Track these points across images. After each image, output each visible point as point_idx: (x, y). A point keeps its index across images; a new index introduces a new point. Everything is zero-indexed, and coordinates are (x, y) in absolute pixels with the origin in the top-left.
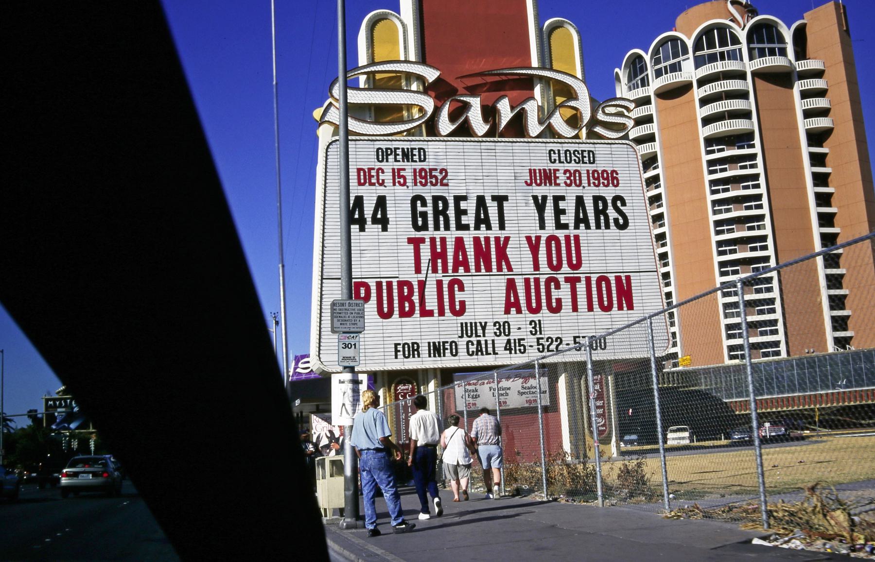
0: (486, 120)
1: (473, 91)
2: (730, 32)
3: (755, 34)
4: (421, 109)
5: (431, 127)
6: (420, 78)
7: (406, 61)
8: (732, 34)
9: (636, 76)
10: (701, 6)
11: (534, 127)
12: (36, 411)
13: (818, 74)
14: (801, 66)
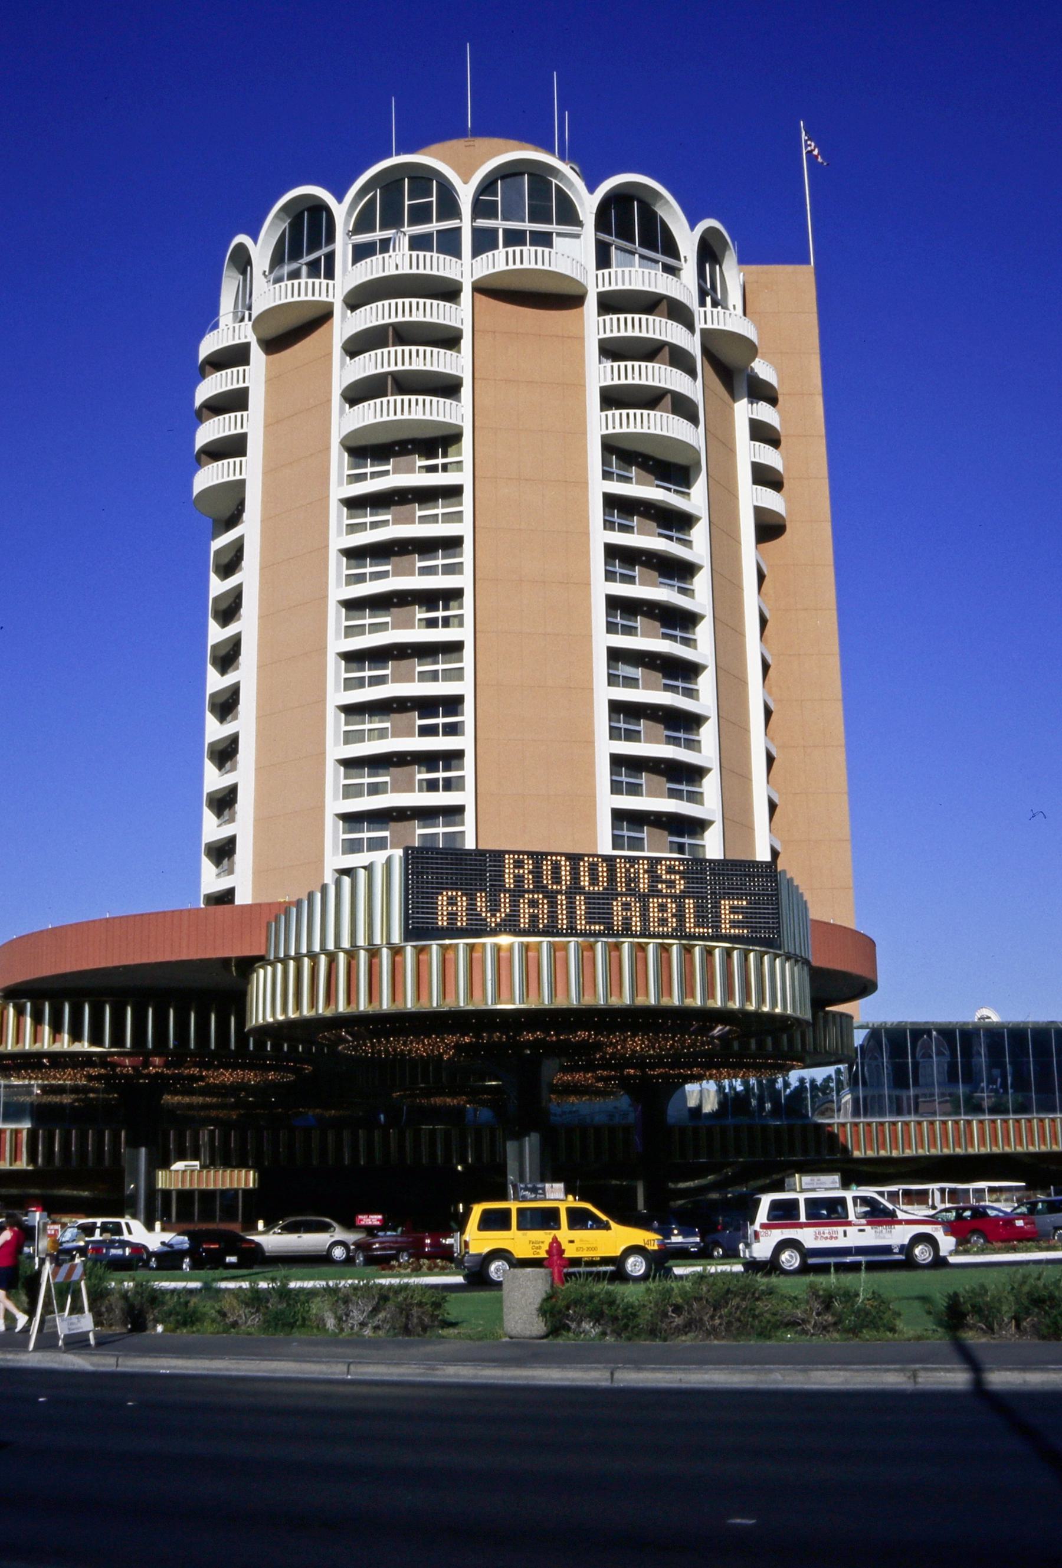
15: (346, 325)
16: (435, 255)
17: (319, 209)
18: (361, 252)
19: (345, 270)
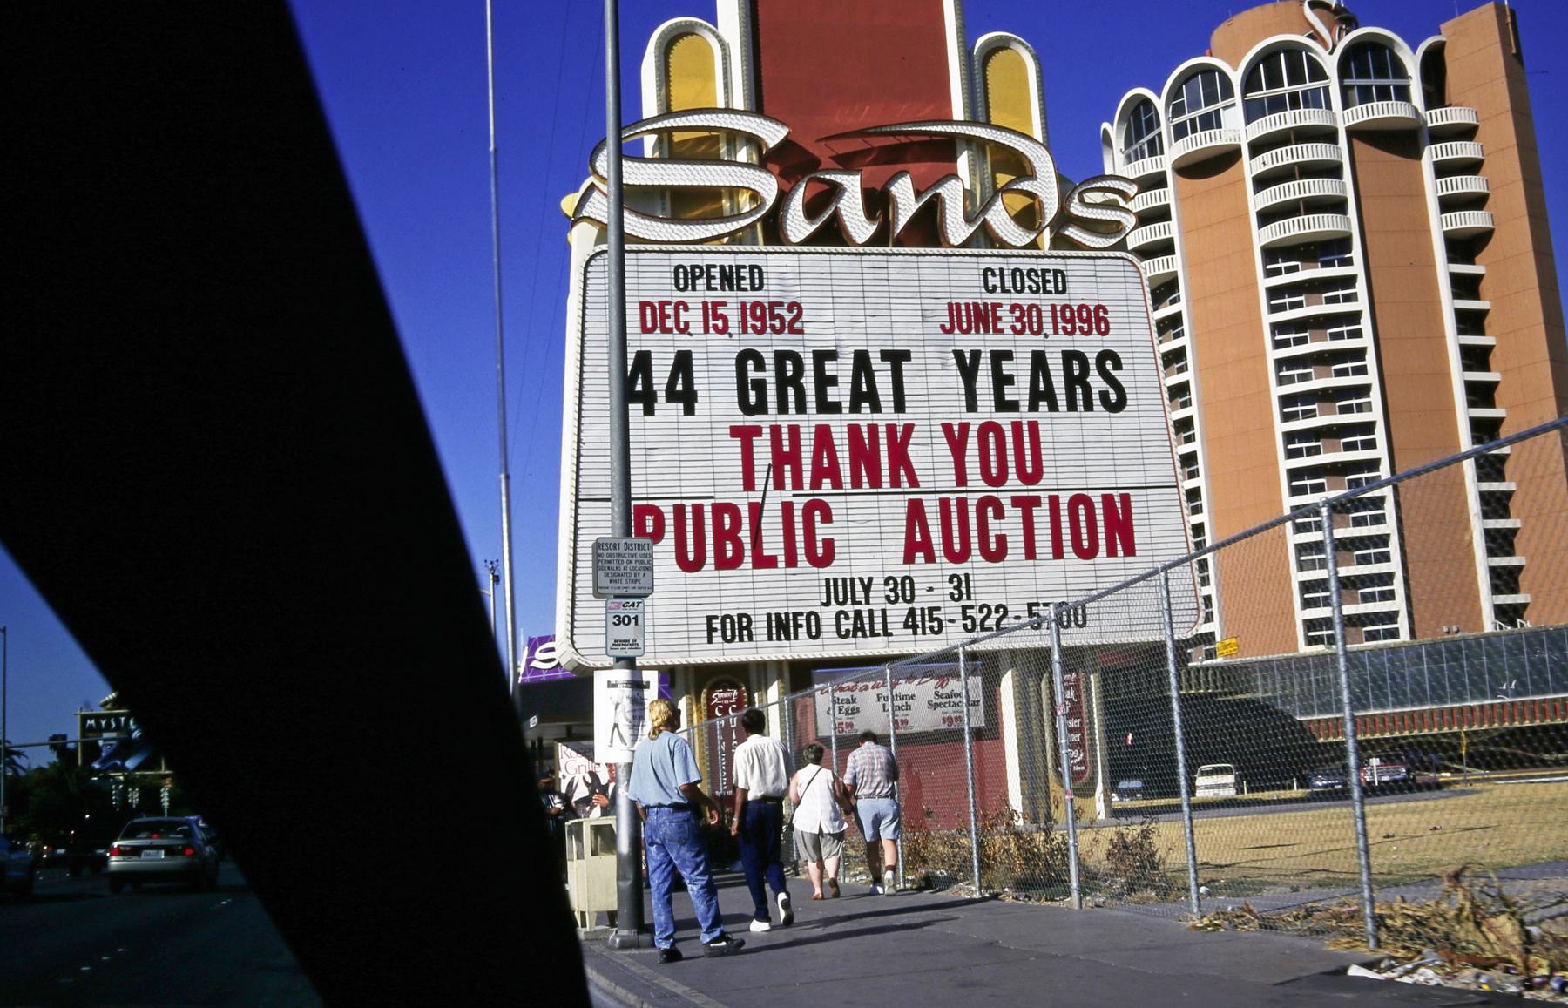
0: (870, 215)
1: (847, 163)
2: (1308, 57)
3: (1353, 60)
4: (755, 196)
5: (773, 227)
6: (753, 141)
7: (728, 110)
8: (1311, 61)
9: (1139, 136)
10: (1257, 10)
11: (957, 228)
12: (64, 737)
13: (1466, 133)
14: (1436, 118)
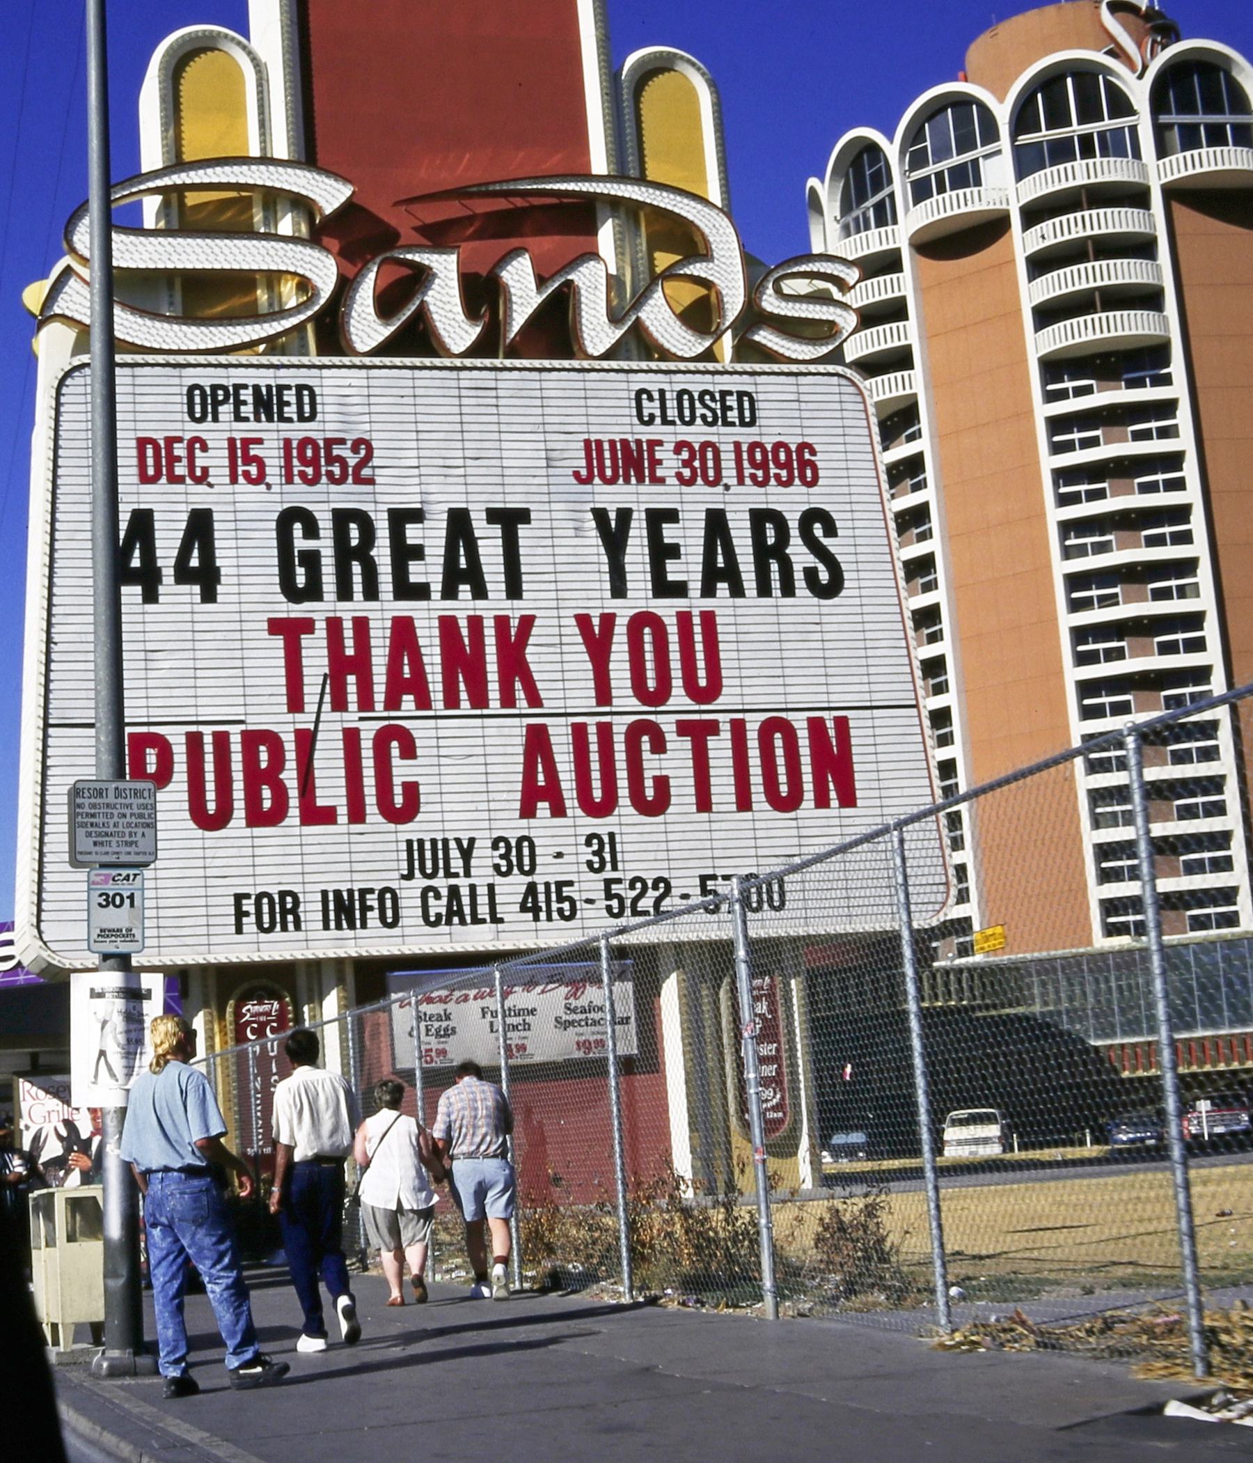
0: (471, 312)
3: (1173, 87)
4: (304, 285)
5: (330, 331)
6: (302, 204)
7: (266, 160)
11: (598, 332)
15: (1024, 242)
16: (1098, 159)
17: (872, 149)
18: (921, 191)
19: (907, 210)
